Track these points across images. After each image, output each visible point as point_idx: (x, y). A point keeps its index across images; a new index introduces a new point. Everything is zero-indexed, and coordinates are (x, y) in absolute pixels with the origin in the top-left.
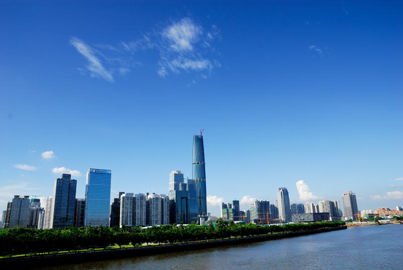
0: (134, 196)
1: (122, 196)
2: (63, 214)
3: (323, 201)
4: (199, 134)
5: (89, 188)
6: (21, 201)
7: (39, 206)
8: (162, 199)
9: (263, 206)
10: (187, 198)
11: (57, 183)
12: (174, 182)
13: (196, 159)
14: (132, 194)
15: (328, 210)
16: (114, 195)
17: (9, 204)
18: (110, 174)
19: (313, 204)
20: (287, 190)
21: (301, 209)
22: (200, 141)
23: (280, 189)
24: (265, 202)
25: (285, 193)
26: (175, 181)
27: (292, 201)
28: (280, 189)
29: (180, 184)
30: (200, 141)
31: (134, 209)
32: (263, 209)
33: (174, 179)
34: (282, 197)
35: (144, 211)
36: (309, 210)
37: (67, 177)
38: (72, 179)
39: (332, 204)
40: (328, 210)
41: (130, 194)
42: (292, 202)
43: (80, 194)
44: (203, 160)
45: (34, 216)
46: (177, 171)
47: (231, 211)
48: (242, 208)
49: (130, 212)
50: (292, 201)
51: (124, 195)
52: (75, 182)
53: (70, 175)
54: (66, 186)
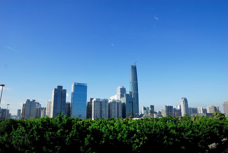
0: (101, 100)
1: (93, 101)
2: (58, 111)
3: (210, 106)
4: (134, 65)
5: (74, 95)
6: (31, 103)
7: (41, 106)
8: (118, 103)
9: (169, 109)
10: (132, 102)
11: (55, 91)
12: (120, 93)
13: (133, 79)
14: (100, 99)
15: (213, 111)
16: (88, 100)
17: (24, 104)
18: (87, 86)
19: (202, 108)
20: (186, 99)
21: (195, 111)
22: (134, 69)
23: (182, 98)
24: (171, 106)
25: (186, 101)
26: (121, 92)
27: (190, 106)
28: (182, 98)
29: (125, 94)
30: (134, 69)
31: (101, 108)
32: (169, 110)
33: (120, 92)
34: (184, 103)
35: (107, 110)
36: (200, 112)
37: (60, 87)
38: (63, 89)
39: (215, 108)
40: (213, 111)
41: (98, 99)
42: (189, 107)
43: (69, 99)
44: (137, 80)
45: (38, 112)
46: (122, 86)
47: (149, 111)
48: (156, 110)
49: (99, 111)
50: (190, 106)
51: (95, 100)
52: (65, 91)
53: (62, 86)
54: (60, 93)
